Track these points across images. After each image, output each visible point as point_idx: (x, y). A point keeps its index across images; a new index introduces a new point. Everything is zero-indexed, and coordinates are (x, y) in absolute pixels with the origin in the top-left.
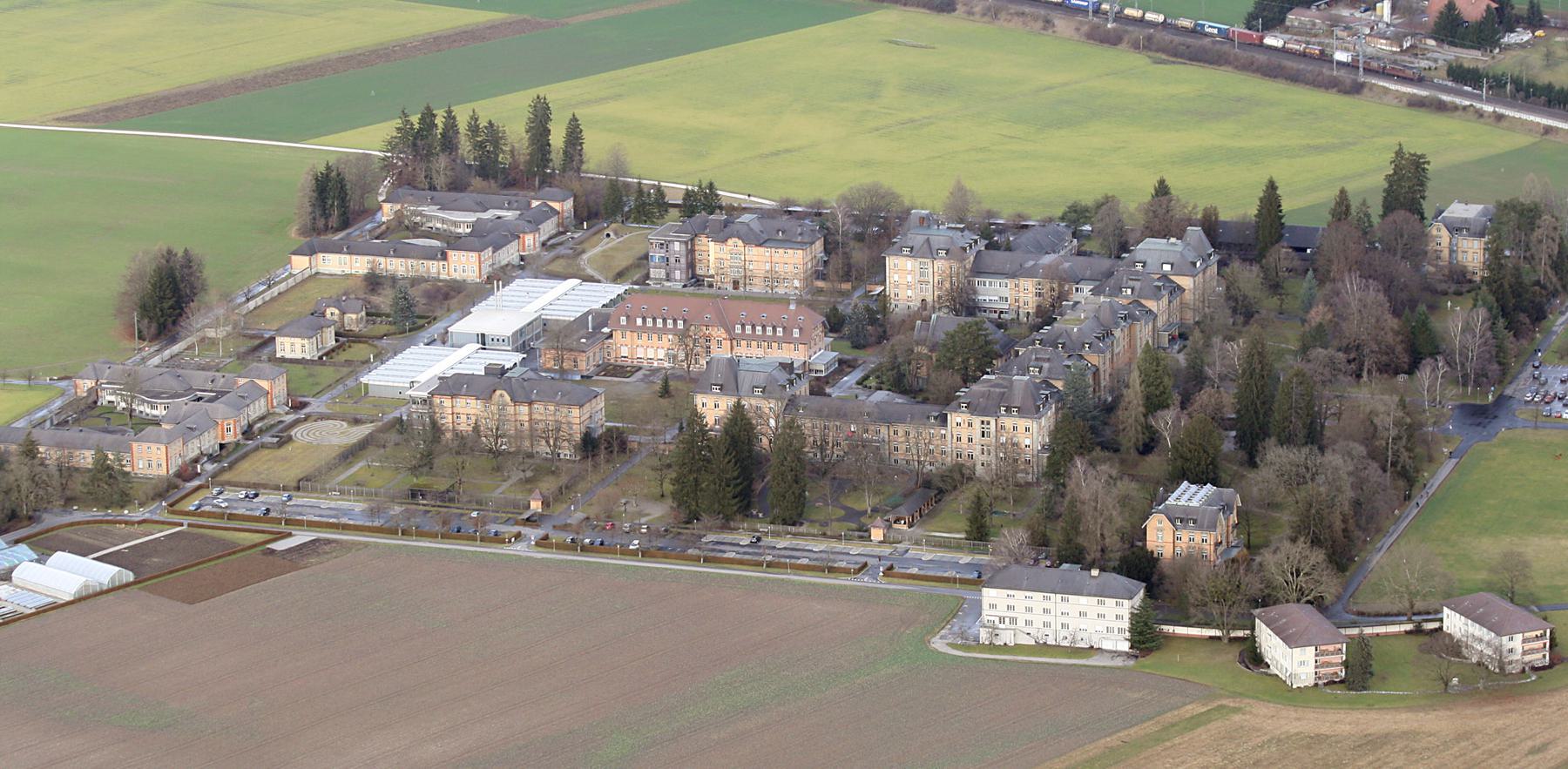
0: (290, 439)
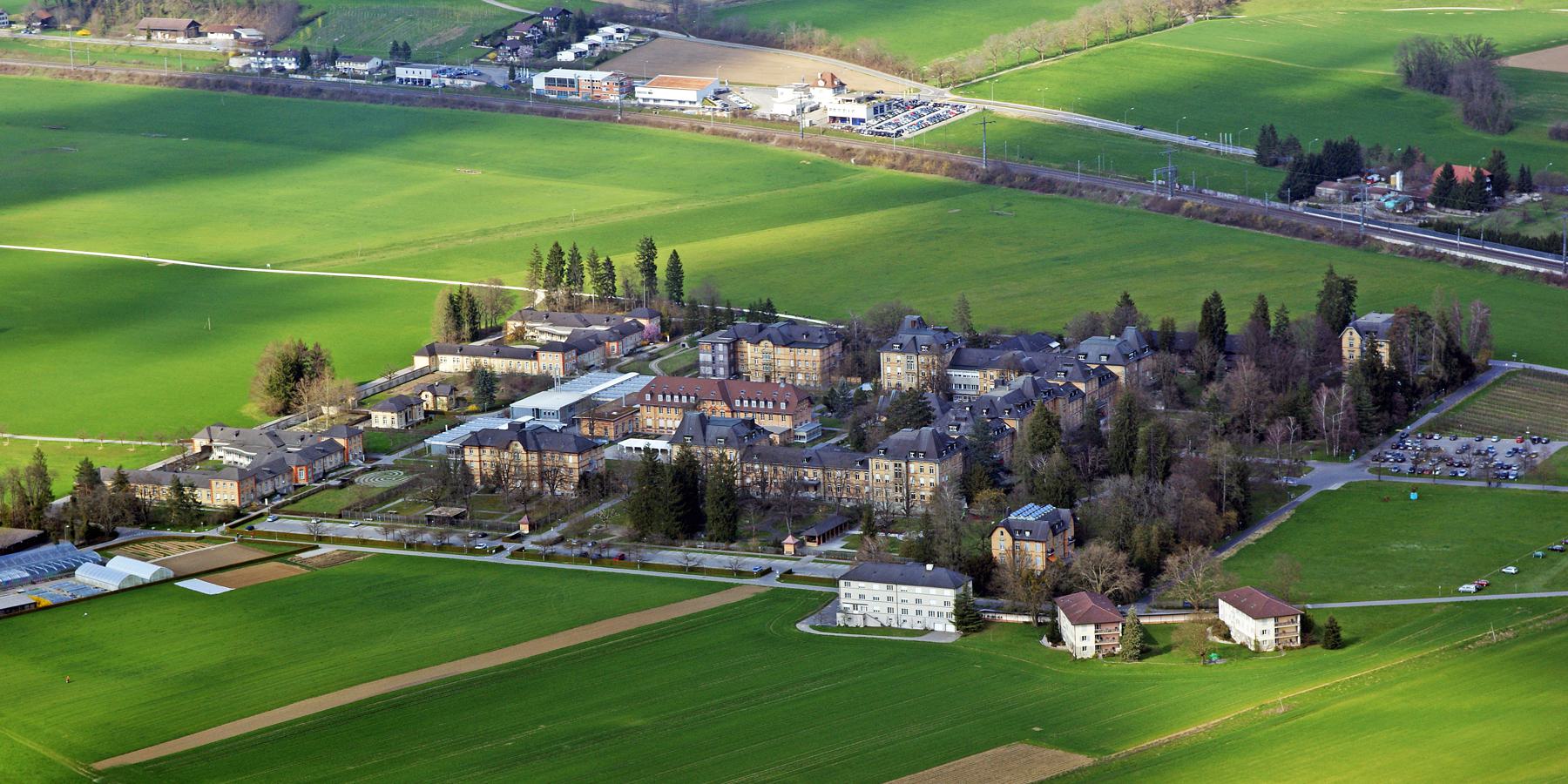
0: (352, 483)
